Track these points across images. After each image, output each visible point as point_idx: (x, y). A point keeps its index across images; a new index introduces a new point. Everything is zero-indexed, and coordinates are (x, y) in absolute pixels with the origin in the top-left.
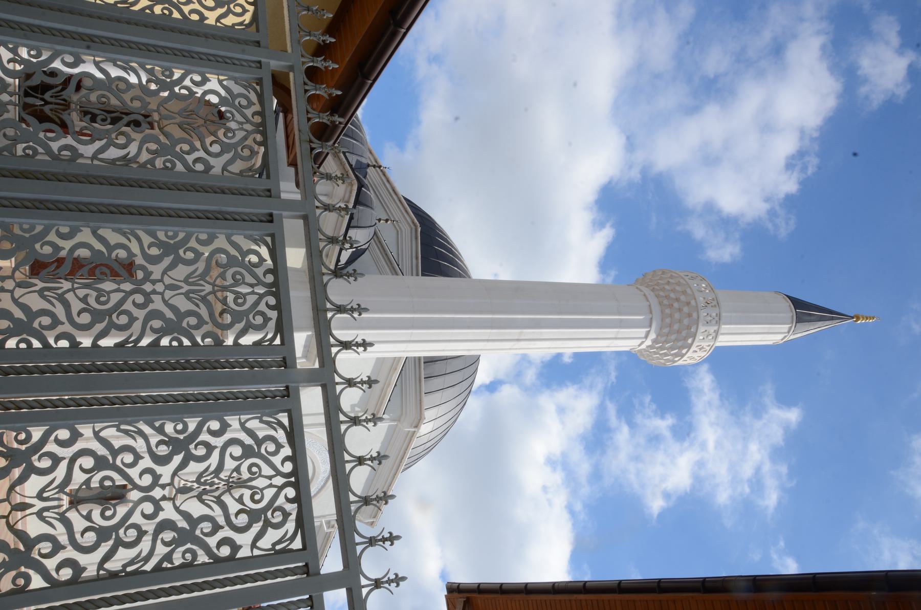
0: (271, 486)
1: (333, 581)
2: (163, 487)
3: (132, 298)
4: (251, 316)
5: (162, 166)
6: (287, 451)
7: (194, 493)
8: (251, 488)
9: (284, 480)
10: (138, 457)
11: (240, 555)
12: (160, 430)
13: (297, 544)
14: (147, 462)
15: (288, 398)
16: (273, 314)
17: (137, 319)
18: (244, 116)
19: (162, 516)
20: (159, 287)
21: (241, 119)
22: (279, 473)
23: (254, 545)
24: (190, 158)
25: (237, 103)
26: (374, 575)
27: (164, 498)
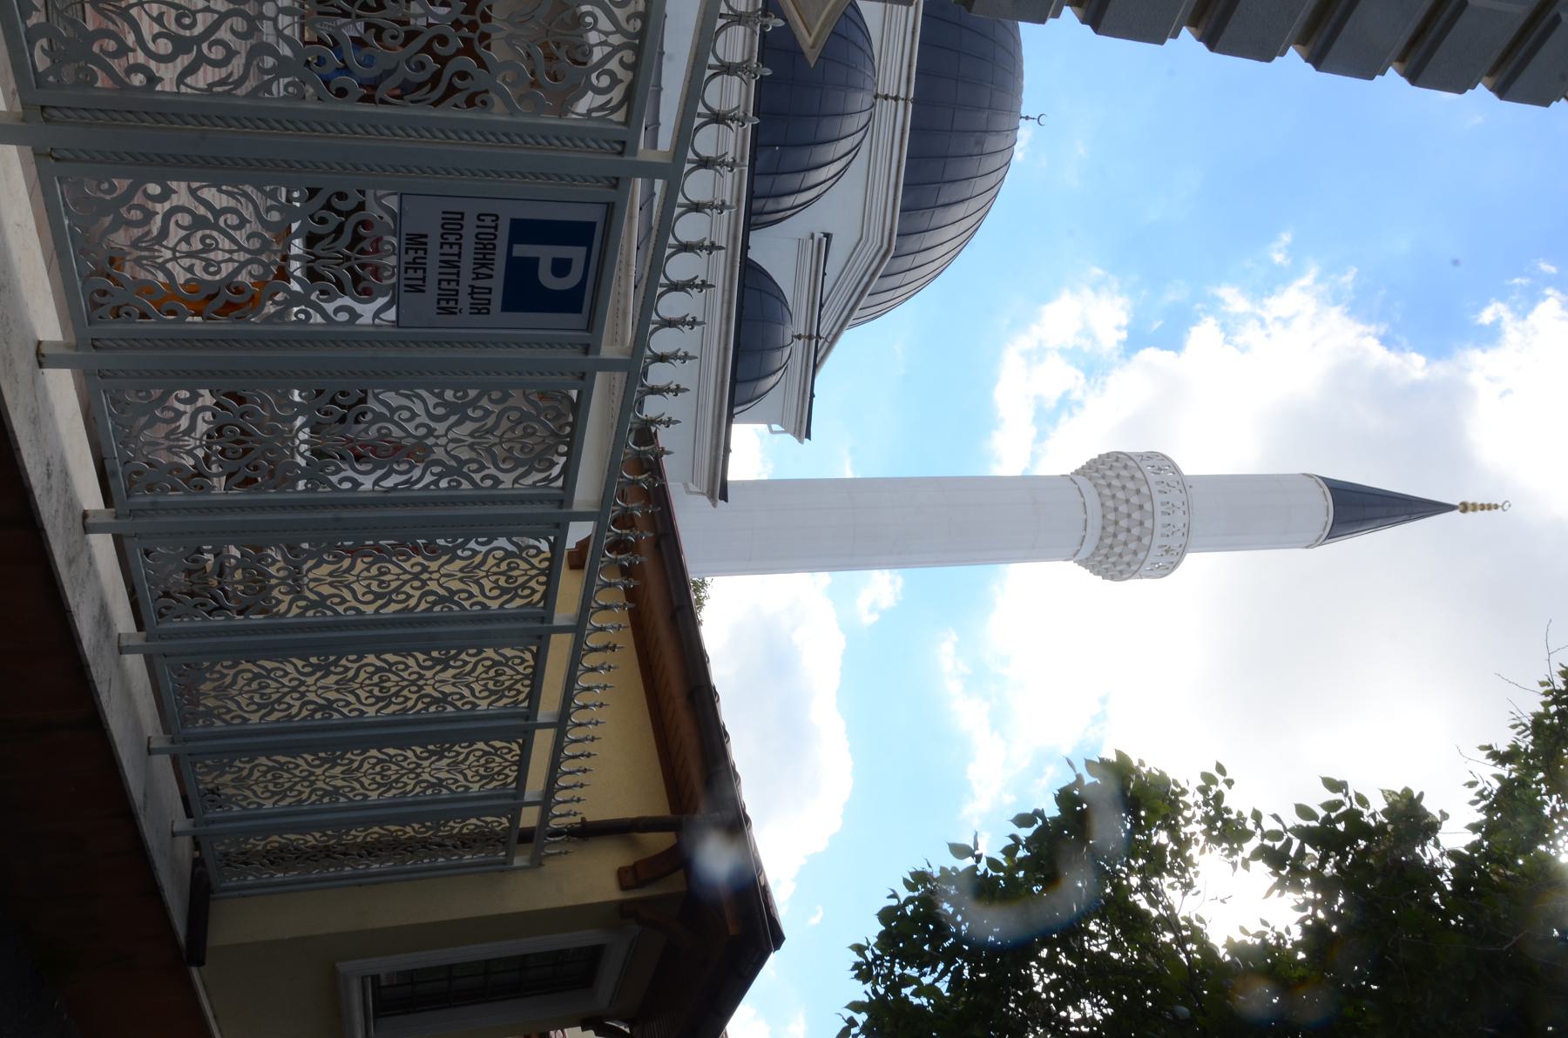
1: (650, 171)
4: (594, 76)
9: (248, 256)
10: (243, 222)
13: (619, 116)
14: (416, 669)
16: (542, 589)
18: (233, 240)
24: (118, 65)
25: (221, 223)
26: (658, 351)
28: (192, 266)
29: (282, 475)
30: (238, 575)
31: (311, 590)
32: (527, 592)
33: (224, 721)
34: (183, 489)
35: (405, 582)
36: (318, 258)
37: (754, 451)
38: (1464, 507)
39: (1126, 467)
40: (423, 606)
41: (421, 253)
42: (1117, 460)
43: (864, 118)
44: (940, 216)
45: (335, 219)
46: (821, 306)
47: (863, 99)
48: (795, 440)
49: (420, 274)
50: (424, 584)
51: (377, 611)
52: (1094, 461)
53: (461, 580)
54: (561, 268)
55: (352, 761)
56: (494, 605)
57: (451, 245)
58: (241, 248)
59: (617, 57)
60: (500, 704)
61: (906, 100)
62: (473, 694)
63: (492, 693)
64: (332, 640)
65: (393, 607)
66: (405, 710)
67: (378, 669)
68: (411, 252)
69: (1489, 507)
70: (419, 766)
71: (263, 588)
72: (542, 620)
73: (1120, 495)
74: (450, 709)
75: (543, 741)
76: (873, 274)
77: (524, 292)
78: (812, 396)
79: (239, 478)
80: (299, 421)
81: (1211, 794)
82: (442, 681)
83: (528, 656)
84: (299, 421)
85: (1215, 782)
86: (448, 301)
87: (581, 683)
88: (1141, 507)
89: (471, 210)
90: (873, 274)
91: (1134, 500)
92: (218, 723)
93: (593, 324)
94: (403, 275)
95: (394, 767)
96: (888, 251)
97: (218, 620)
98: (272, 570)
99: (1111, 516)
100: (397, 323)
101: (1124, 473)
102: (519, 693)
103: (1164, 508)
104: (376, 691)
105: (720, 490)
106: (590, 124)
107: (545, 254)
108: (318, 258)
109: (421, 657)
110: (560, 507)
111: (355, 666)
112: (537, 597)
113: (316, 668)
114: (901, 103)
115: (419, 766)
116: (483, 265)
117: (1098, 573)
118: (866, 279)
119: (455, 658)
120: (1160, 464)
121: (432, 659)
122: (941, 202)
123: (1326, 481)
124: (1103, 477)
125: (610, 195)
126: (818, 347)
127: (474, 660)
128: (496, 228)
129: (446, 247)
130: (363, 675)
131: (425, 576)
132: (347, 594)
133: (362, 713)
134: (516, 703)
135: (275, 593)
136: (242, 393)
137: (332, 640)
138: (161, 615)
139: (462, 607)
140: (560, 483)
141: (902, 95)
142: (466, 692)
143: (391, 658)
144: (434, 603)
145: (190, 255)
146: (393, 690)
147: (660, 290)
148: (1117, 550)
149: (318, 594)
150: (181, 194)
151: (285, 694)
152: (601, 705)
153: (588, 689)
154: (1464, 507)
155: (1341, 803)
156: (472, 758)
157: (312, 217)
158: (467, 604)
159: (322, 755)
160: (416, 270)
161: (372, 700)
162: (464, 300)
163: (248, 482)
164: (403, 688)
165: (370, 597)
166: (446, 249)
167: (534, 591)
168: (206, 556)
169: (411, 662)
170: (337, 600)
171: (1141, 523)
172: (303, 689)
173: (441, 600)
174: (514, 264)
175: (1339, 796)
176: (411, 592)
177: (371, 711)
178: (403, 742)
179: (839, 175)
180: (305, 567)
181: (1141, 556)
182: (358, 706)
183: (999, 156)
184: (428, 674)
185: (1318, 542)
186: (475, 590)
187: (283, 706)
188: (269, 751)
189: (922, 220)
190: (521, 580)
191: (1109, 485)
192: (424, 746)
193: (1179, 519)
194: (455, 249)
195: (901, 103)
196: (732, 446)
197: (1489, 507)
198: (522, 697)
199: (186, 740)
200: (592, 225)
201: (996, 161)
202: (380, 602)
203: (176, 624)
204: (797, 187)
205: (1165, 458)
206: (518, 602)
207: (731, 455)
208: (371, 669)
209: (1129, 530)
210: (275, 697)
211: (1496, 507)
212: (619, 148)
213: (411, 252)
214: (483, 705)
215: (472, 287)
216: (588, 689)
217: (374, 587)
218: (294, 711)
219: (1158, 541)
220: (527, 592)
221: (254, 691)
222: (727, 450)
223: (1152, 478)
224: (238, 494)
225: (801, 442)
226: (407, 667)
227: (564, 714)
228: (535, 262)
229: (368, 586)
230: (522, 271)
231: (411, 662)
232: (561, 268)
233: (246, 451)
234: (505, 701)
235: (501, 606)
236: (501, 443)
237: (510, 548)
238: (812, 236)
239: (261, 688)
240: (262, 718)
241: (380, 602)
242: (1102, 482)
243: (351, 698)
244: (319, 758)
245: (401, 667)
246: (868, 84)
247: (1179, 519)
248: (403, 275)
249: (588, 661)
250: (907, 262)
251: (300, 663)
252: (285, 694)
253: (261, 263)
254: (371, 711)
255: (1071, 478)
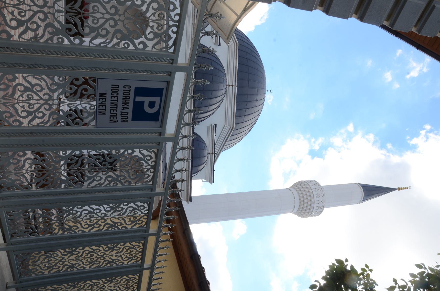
0: (103, 18)
1: (169, 139)
2: (120, 15)
3: (44, 106)
4: (100, 30)
5: (56, 42)
6: (178, 11)
7: (66, 104)
8: (90, 104)
9: (110, 17)
10: (42, 89)
11: (147, 49)
12: (53, 79)
14: (103, 251)
15: (145, 239)
16: (152, 175)
17: (46, 115)
18: (105, 8)
19: (117, 27)
20: (51, 10)
21: (104, 11)
22: (149, 165)
23: (153, 47)
24: (137, 41)
27: (119, 20)
28: (24, 106)
29: (56, 183)
30: (41, 220)
31: (66, 224)
32: (140, 222)
33: (35, 274)
34: (21, 189)
35: (99, 220)
36: (70, 170)
37: (199, 187)
38: (399, 189)
39: (304, 185)
40: (105, 228)
41: (104, 100)
42: (302, 183)
43: (224, 91)
44: (246, 118)
45: (74, 88)
46: (215, 145)
47: (223, 86)
48: (209, 184)
49: (104, 108)
50: (105, 220)
51: (89, 231)
52: (295, 184)
53: (118, 219)
54: (152, 105)
55: (81, 286)
56: (129, 227)
57: (115, 97)
58: (41, 99)
59: (108, 23)
60: (132, 262)
61: (235, 86)
62: (123, 260)
63: (129, 258)
64: (75, 242)
65: (95, 229)
66: (99, 266)
67: (90, 252)
68: (101, 100)
69: (406, 188)
70: (104, 286)
71: (49, 224)
72: (146, 232)
73: (304, 193)
74: (114, 265)
75: (146, 274)
76: (229, 135)
77: (139, 114)
78: (214, 170)
79: (40, 184)
80: (62, 162)
81: (365, 275)
82: (112, 255)
83: (141, 245)
84: (62, 162)
85: (366, 271)
86: (113, 117)
87: (159, 253)
88: (310, 196)
89: (121, 84)
90: (229, 135)
91: (308, 194)
92: (33, 275)
93: (163, 125)
94: (98, 108)
95: (95, 287)
96: (233, 128)
97: (33, 237)
98: (53, 218)
99: (302, 199)
100: (96, 126)
101: (304, 186)
102: (138, 258)
103: (317, 196)
104: (89, 260)
105: (190, 199)
106: (162, 53)
107: (146, 100)
108: (70, 170)
109: (104, 247)
110: (152, 191)
111: (82, 251)
112: (144, 224)
113: (68, 252)
114: (234, 87)
115: (104, 286)
116: (125, 104)
117: (300, 216)
118: (227, 136)
119: (116, 247)
120: (314, 183)
121: (108, 247)
122: (246, 114)
123: (360, 184)
124: (299, 188)
125: (169, 78)
126: (215, 156)
127: (122, 247)
128: (130, 90)
129: (113, 98)
130: (84, 254)
131: (106, 218)
132: (79, 225)
133: (84, 268)
134: (137, 262)
135: (54, 226)
136: (42, 153)
137: (75, 242)
138: (12, 236)
139: (118, 228)
140: (151, 183)
141: (234, 85)
142: (120, 259)
143: (94, 248)
144: (109, 227)
145: (23, 101)
146: (95, 259)
147: (185, 112)
148: (305, 209)
149: (69, 226)
150: (20, 78)
151: (57, 263)
152: (165, 260)
153: (161, 255)
154: (399, 189)
155: (424, 272)
156: (122, 282)
157: (69, 159)
158: (120, 227)
159: (70, 284)
160: (102, 106)
161: (88, 263)
162: (119, 117)
163: (43, 186)
164: (99, 258)
165: (87, 226)
166: (113, 98)
167: (143, 222)
168: (30, 213)
169: (101, 249)
170: (75, 228)
171: (311, 200)
172: (63, 260)
173: (111, 226)
174: (135, 103)
175: (423, 270)
176: (101, 224)
177: (87, 267)
178: (98, 278)
179: (218, 107)
180: (65, 215)
181: (312, 210)
182: (83, 266)
183: (261, 101)
184: (107, 253)
185: (361, 202)
186: (123, 222)
187: (57, 267)
188: (51, 284)
189: (241, 119)
190: (138, 218)
191: (300, 190)
192: (105, 278)
193: (321, 199)
194: (116, 99)
195: (234, 87)
196: (192, 186)
197: (406, 188)
198: (139, 259)
199: (21, 282)
200: (163, 89)
201: (261, 102)
202: (90, 228)
203: (18, 239)
204: (206, 111)
205: (315, 181)
206: (137, 226)
207: (192, 188)
208: (87, 252)
209: (307, 203)
210: (53, 264)
211: (407, 188)
212: (171, 61)
213: (101, 100)
214: (126, 263)
215: (122, 112)
216: (161, 255)
217: (88, 222)
218: (60, 269)
219: (316, 205)
220: (140, 222)
221: (46, 262)
222: (191, 187)
223: (312, 187)
224: (41, 190)
225: (212, 184)
226: (100, 251)
227: (153, 265)
228: (143, 103)
229: (86, 222)
230: (138, 106)
231: (101, 249)
232: (152, 105)
233: (43, 174)
234: (133, 261)
235: (132, 227)
236: (131, 169)
237: (135, 206)
238: (211, 125)
239: (49, 261)
240: (49, 272)
241: (90, 228)
242: (298, 189)
243: (81, 263)
244: (69, 285)
245: (98, 251)
246: (225, 82)
247: (321, 199)
248: (98, 108)
249: (161, 246)
250: (238, 131)
251: (62, 251)
252: (57, 263)
253: (48, 104)
254: (87, 267)
255: (290, 189)
